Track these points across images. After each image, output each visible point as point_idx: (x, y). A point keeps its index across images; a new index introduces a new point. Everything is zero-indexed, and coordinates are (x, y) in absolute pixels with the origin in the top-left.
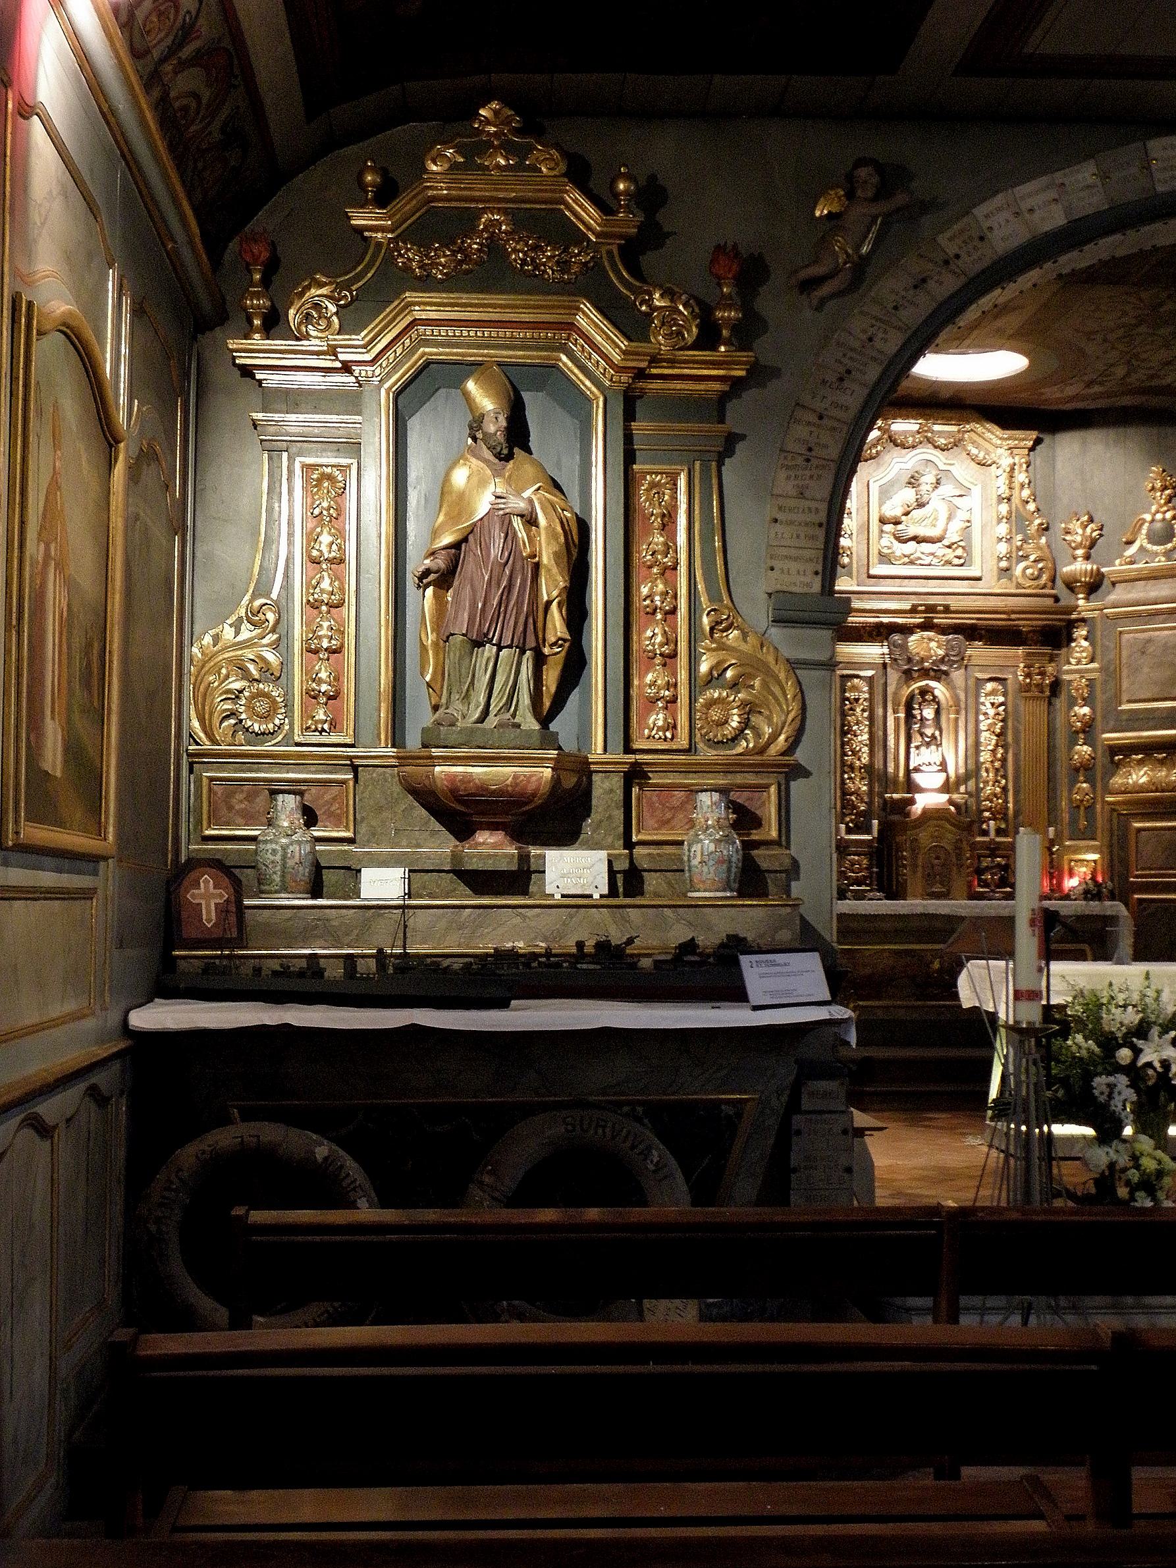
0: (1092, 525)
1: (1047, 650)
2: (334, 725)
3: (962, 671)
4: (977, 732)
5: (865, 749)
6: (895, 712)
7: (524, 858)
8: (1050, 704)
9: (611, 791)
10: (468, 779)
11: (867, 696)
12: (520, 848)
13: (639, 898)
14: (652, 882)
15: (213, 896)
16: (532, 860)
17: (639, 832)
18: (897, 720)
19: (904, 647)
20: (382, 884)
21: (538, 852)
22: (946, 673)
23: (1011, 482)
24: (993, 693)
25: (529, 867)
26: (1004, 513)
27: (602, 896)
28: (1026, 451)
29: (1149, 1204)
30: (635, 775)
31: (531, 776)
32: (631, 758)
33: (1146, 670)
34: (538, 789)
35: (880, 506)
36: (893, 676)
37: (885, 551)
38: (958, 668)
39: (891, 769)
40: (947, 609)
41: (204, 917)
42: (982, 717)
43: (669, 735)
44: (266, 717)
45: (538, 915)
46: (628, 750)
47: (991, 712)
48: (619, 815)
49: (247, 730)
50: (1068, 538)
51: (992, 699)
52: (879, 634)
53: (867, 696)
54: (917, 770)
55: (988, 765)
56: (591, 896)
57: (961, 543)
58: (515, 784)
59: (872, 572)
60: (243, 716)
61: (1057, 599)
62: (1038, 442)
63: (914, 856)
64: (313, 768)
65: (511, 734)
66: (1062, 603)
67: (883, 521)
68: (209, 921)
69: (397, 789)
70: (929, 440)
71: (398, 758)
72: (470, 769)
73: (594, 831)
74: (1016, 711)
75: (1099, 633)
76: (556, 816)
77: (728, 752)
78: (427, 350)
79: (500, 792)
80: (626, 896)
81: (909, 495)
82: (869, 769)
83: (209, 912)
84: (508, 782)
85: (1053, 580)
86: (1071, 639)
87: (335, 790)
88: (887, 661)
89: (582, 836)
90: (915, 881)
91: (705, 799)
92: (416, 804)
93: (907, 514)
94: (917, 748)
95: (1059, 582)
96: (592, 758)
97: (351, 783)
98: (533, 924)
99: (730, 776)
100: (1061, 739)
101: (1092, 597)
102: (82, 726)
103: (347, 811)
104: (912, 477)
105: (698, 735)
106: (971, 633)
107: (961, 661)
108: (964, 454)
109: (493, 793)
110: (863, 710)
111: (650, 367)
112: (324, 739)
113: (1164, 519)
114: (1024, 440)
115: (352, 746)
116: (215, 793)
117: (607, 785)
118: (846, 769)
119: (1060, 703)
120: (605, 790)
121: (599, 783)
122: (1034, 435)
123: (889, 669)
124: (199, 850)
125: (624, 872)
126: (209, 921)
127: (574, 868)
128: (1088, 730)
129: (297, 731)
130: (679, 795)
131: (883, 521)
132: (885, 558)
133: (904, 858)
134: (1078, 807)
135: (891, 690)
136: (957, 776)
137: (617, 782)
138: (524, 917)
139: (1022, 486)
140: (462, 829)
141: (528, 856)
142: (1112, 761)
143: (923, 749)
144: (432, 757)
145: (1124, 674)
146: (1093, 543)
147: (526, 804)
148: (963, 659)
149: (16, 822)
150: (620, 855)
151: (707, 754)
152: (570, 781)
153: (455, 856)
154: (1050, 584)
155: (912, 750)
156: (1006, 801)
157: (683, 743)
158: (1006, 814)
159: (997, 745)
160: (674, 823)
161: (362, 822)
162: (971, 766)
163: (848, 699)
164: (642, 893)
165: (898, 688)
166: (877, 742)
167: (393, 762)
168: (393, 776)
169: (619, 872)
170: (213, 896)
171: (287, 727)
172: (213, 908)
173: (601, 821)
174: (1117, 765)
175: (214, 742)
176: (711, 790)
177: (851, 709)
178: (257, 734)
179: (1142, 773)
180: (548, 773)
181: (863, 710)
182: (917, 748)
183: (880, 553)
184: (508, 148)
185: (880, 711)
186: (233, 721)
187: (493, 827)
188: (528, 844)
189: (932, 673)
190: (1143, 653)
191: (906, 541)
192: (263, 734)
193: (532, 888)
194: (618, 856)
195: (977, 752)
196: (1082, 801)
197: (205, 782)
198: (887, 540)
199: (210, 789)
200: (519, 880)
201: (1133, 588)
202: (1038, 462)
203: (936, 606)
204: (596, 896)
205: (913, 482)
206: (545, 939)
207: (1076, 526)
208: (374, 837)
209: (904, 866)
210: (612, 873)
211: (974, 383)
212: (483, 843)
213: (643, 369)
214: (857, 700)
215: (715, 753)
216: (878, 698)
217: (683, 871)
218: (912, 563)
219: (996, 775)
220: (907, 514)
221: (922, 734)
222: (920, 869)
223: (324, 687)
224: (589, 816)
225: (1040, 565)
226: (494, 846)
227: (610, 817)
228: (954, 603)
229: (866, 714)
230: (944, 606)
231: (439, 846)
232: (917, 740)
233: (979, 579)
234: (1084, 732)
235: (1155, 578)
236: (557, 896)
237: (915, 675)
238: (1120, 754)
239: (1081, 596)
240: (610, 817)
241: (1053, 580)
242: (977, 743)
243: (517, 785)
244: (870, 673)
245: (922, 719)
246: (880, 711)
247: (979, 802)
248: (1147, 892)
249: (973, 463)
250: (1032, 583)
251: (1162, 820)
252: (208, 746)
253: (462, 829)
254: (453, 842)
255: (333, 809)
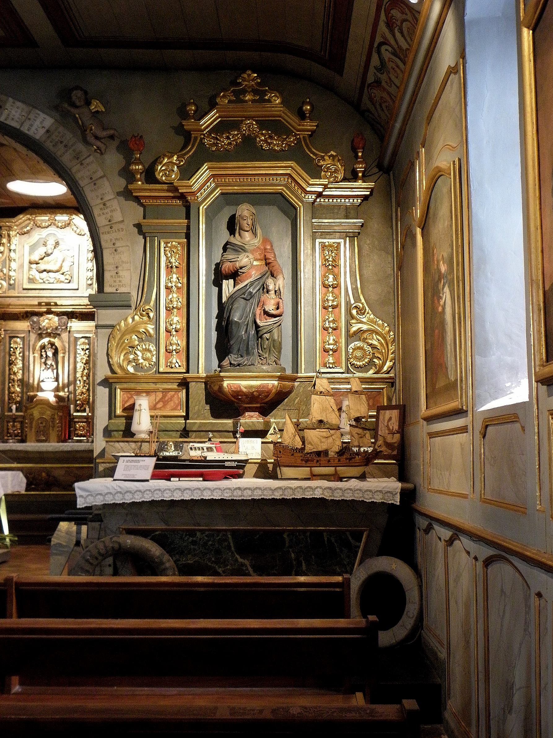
4: (75, 362)
11: (21, 346)
19: (38, 323)
22: (59, 335)
24: (84, 343)
36: (33, 336)
39: (31, 381)
40: (56, 305)
42: (78, 355)
47: (82, 353)
51: (83, 347)
52: (27, 317)
53: (21, 346)
54: (43, 381)
55: (80, 378)
63: (31, 423)
67: (31, 263)
70: (55, 225)
78: (285, 189)
82: (21, 381)
90: (31, 435)
93: (42, 259)
111: (323, 191)
118: (11, 381)
123: (31, 333)
131: (31, 263)
135: (32, 343)
136: (63, 384)
156: (89, 396)
158: (88, 402)
162: (71, 378)
163: (12, 348)
165: (35, 342)
166: (25, 368)
183: (29, 278)
184: (255, 92)
198: (34, 273)
203: (50, 303)
209: (27, 427)
211: (47, 197)
213: (322, 192)
216: (26, 347)
219: (84, 383)
222: (33, 429)
223: (331, 347)
230: (54, 303)
237: (44, 336)
244: (23, 335)
245: (47, 356)
247: (75, 396)
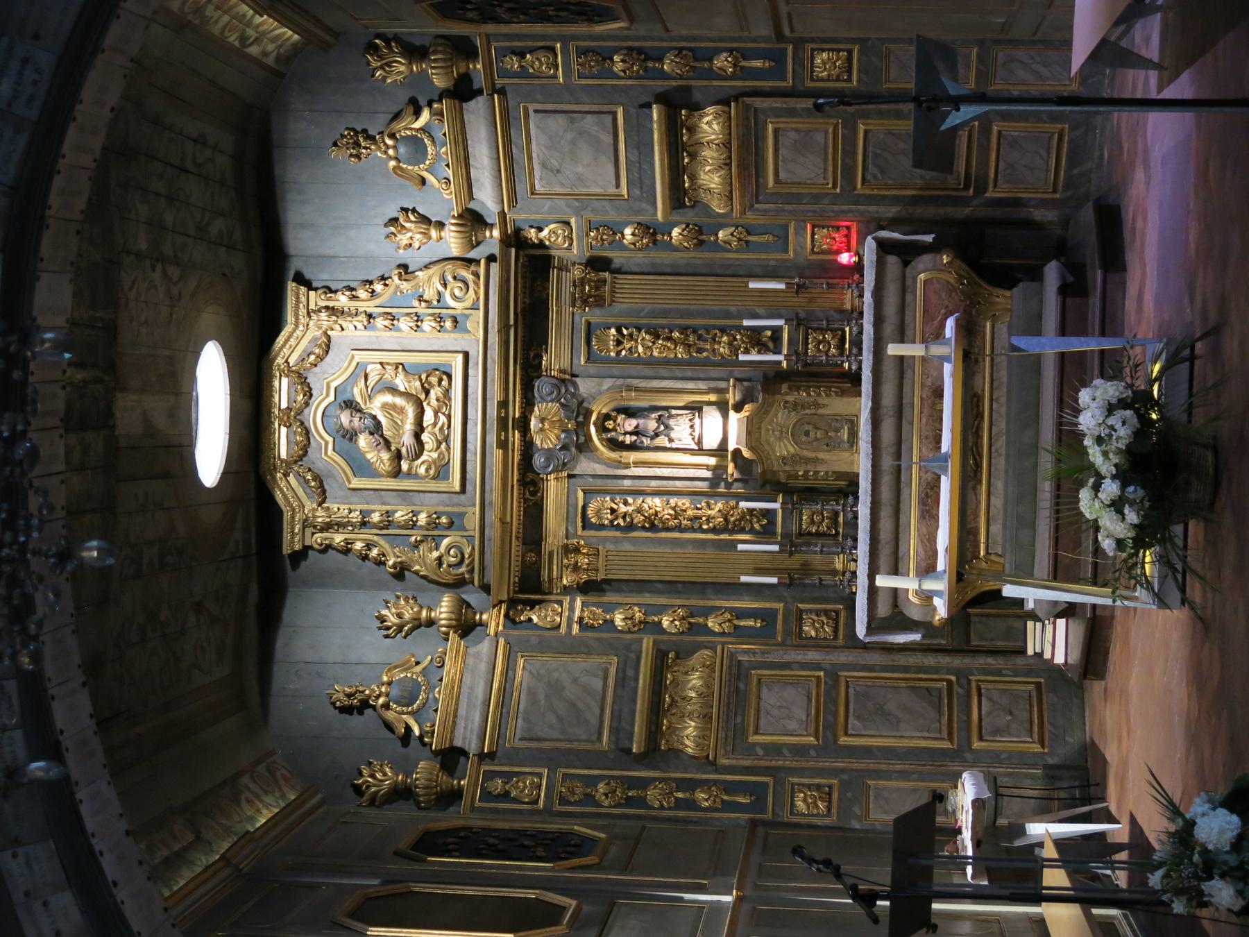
0: (401, 220)
1: (554, 274)
3: (578, 380)
5: (673, 501)
6: (627, 466)
8: (619, 271)
18: (637, 464)
19: (549, 454)
23: (350, 314)
26: (387, 323)
28: (312, 293)
29: (1159, 873)
33: (580, 169)
35: (380, 476)
36: (585, 466)
37: (432, 472)
38: (575, 385)
40: (503, 404)
50: (416, 245)
54: (699, 442)
57: (424, 377)
59: (457, 488)
61: (491, 259)
62: (301, 279)
66: (496, 250)
74: (629, 314)
75: (533, 217)
81: (363, 441)
85: (469, 262)
86: (541, 245)
88: (565, 474)
90: (835, 461)
94: (671, 440)
95: (472, 254)
100: (663, 258)
101: (489, 221)
102: (799, 70)
104: (344, 437)
106: (531, 370)
107: (566, 380)
108: (315, 369)
110: (626, 503)
113: (395, 147)
114: (298, 298)
118: (696, 526)
119: (618, 258)
122: (291, 286)
128: (651, 232)
131: (396, 473)
132: (441, 471)
133: (806, 472)
134: (747, 242)
135: (600, 469)
139: (354, 298)
142: (693, 207)
143: (673, 435)
145: (584, 190)
146: (425, 220)
148: (563, 381)
149: (847, 717)
154: (473, 268)
155: (674, 445)
159: (669, 339)
163: (612, 522)
174: (696, 203)
177: (624, 517)
179: (705, 127)
181: (626, 503)
182: (671, 440)
183: (435, 478)
185: (627, 483)
189: (581, 419)
190: (558, 171)
191: (421, 444)
195: (677, 362)
196: (740, 239)
201: (478, 180)
202: (325, 276)
205: (351, 435)
207: (404, 239)
209: (816, 473)
214: (613, 511)
218: (447, 439)
220: (387, 444)
221: (657, 435)
225: (450, 278)
228: (495, 394)
229: (630, 500)
232: (662, 441)
233: (466, 355)
234: (654, 234)
235: (467, 158)
238: (679, 196)
239: (488, 233)
241: (469, 262)
242: (666, 362)
246: (627, 483)
248: (854, 176)
249: (328, 359)
250: (471, 291)
251: (765, 162)
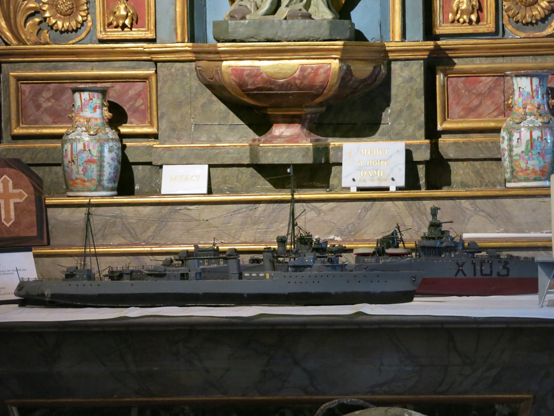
2: (136, 21)
7: (322, 151)
9: (411, 79)
10: (256, 73)
12: (317, 140)
13: (445, 189)
14: (458, 172)
15: (13, 196)
16: (331, 152)
17: (444, 120)
20: (184, 180)
21: (337, 144)
25: (327, 159)
27: (399, 189)
30: (436, 63)
31: (318, 68)
32: (430, 45)
34: (326, 80)
41: (3, 217)
43: (474, 17)
44: (69, 14)
45: (332, 210)
46: (429, 33)
48: (420, 104)
49: (52, 27)
56: (387, 189)
58: (303, 77)
60: (47, 15)
64: (117, 64)
65: (301, 23)
68: (7, 220)
69: (196, 83)
71: (195, 52)
72: (256, 63)
73: (394, 122)
76: (354, 107)
77: (538, 34)
79: (288, 85)
80: (430, 186)
83: (7, 212)
84: (296, 75)
87: (139, 86)
89: (382, 127)
91: (523, 84)
92: (214, 98)
96: (390, 46)
97: (153, 79)
98: (328, 218)
99: (539, 59)
103: (151, 108)
105: (506, 17)
109: (282, 86)
112: (127, 34)
115: (153, 41)
116: (23, 93)
117: (406, 73)
120: (406, 80)
121: (398, 71)
124: (275, 111)
125: (426, 163)
126: (7, 220)
127: (371, 162)
129: (99, 27)
130: (487, 80)
137: (417, 70)
138: (319, 212)
140: (260, 123)
141: (326, 149)
144: (218, 53)
147: (317, 96)
150: (420, 145)
151: (515, 36)
152: (362, 70)
153: (253, 151)
157: (488, 25)
160: (480, 110)
161: (162, 117)
164: (448, 183)
167: (191, 56)
168: (190, 71)
169: (420, 163)
170: (13, 196)
171: (90, 24)
172: (12, 207)
173: (401, 111)
175: (20, 41)
176: (531, 76)
178: (62, 32)
180: (335, 64)
186: (37, 20)
187: (290, 120)
188: (328, 136)
192: (67, 31)
193: (333, 181)
194: (419, 146)
197: (12, 82)
199: (18, 89)
200: (319, 172)
204: (393, 189)
206: (340, 233)
208: (175, 131)
210: (411, 165)
212: (279, 137)
215: (523, 35)
217: (499, 159)
224: (388, 105)
226: (291, 139)
227: (410, 106)
231: (236, 139)
236: (354, 190)
240: (410, 106)
243: (304, 77)
252: (14, 45)
253: (260, 123)
254: (252, 135)
255: (137, 104)
